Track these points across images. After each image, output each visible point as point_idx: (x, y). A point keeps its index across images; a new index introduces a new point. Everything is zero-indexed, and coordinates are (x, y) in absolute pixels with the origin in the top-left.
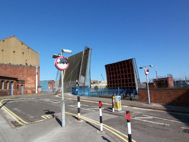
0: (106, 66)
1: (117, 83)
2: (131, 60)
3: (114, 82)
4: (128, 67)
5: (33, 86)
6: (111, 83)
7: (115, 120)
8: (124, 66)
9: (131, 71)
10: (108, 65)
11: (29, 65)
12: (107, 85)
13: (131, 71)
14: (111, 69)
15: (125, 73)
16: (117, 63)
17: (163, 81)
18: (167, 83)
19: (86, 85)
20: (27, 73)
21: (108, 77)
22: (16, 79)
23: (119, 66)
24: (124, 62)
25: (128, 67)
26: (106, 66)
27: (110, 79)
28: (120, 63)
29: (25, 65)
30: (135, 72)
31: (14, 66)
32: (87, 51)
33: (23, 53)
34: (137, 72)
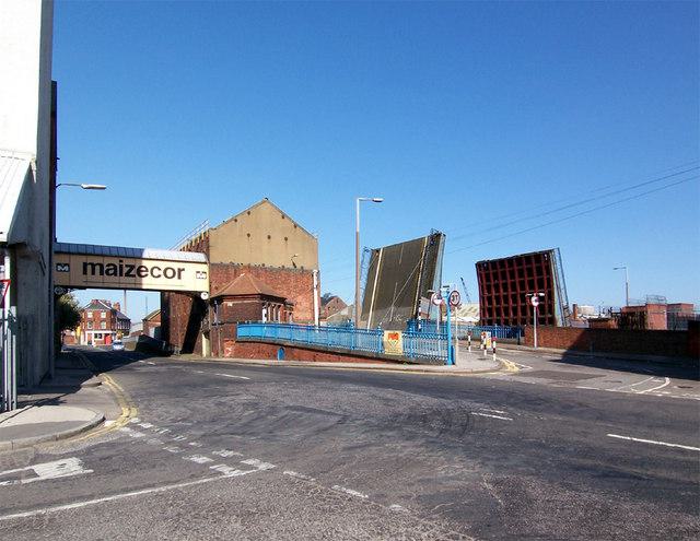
0: (479, 265)
1: (507, 314)
2: (548, 253)
3: (498, 298)
4: (540, 272)
5: (309, 316)
6: (490, 303)
7: (419, 419)
8: (528, 269)
9: (544, 272)
10: (484, 262)
11: (298, 267)
12: (478, 318)
13: (544, 272)
14: (491, 273)
15: (529, 276)
16: (510, 261)
17: (632, 314)
18: (644, 319)
19: (432, 317)
20: (296, 287)
21: (482, 298)
22: (282, 300)
23: (516, 268)
24: (527, 258)
25: (540, 272)
26: (479, 265)
27: (490, 303)
28: (519, 260)
29: (292, 267)
30: (555, 286)
31: (272, 269)
32: (436, 239)
33: (286, 239)
34: (562, 287)
